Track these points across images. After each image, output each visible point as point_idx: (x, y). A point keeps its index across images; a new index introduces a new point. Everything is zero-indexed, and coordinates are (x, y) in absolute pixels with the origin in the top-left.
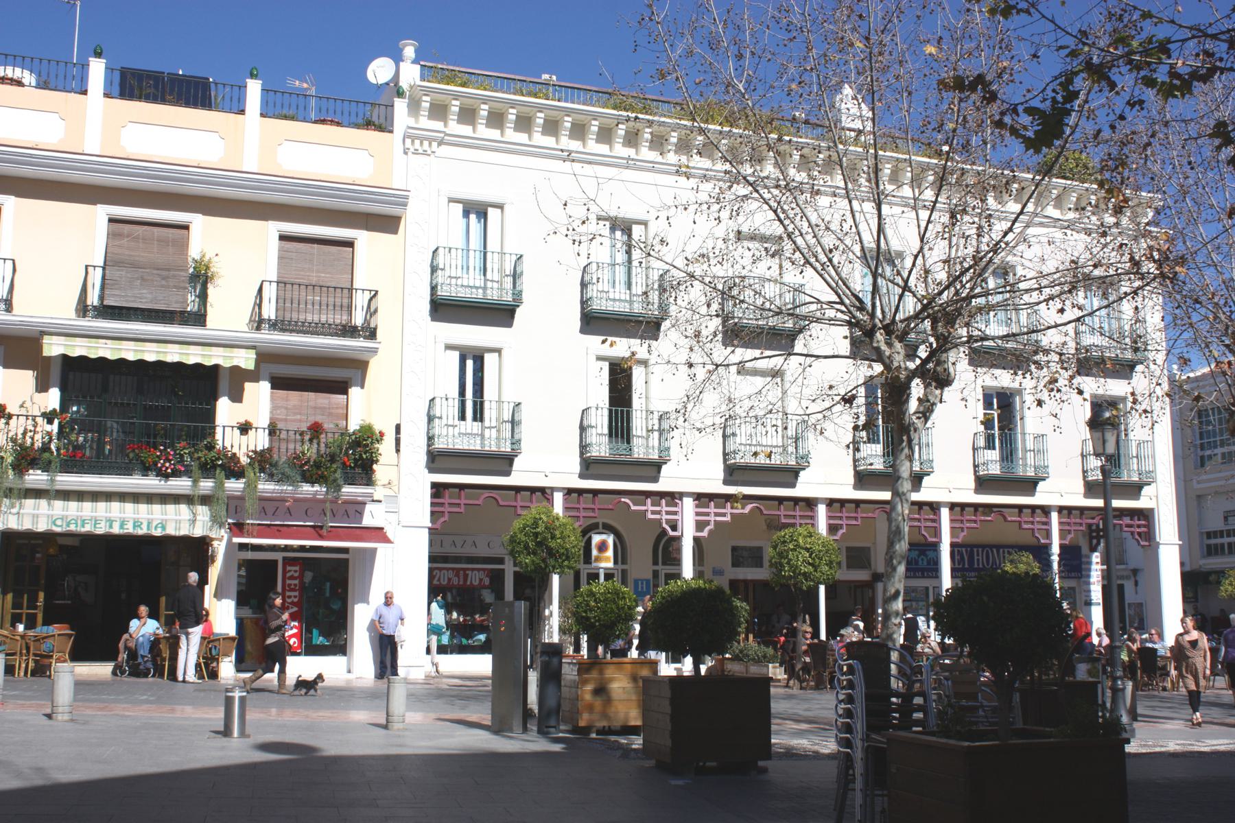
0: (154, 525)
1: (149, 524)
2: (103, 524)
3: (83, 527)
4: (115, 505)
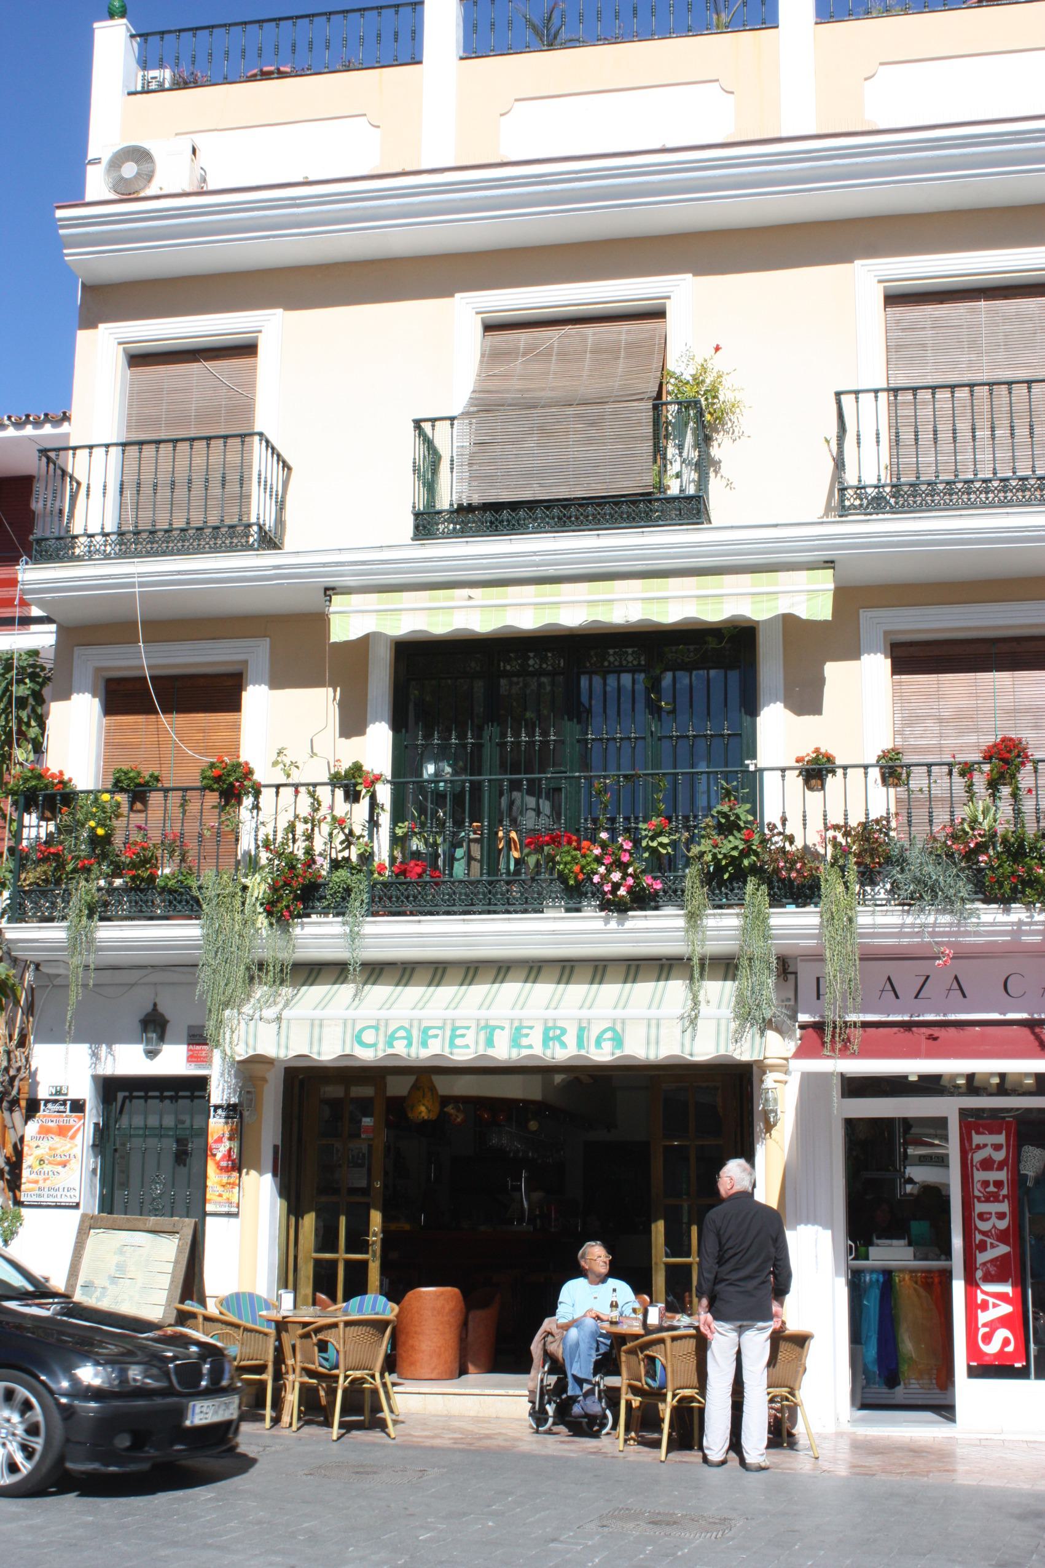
0: (595, 1032)
1: (582, 1032)
2: (470, 1037)
3: (425, 1044)
4: (511, 989)
